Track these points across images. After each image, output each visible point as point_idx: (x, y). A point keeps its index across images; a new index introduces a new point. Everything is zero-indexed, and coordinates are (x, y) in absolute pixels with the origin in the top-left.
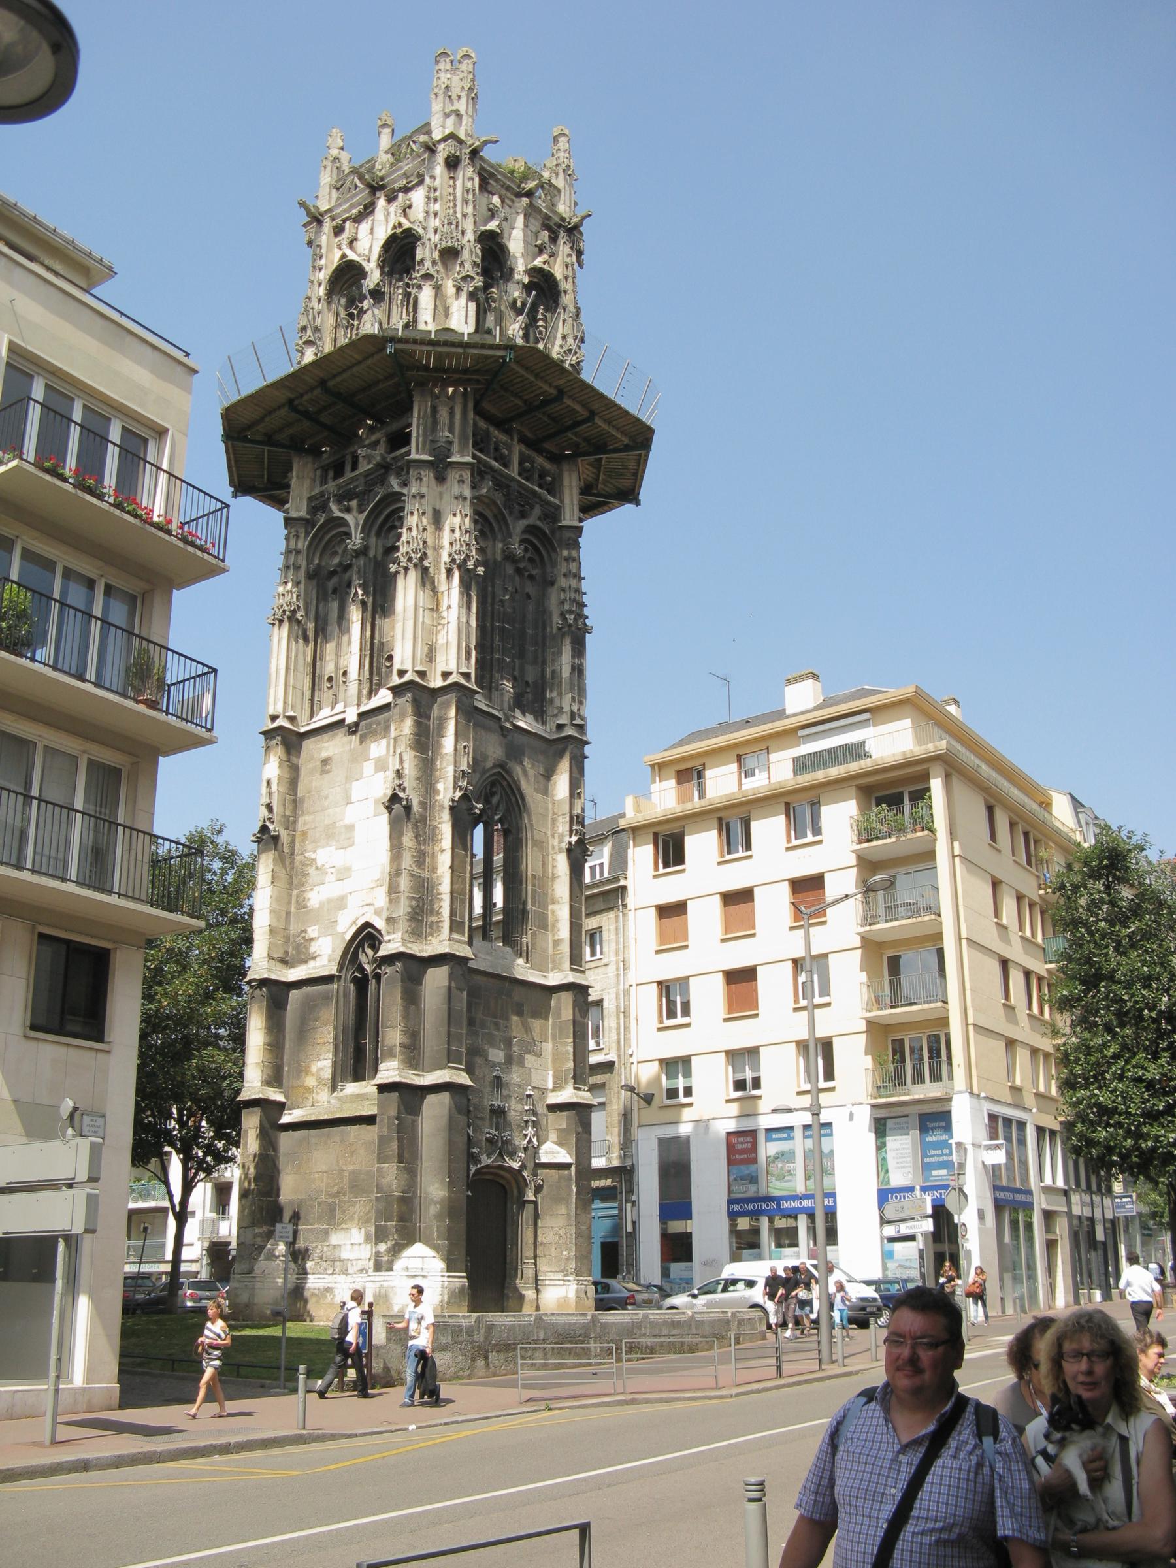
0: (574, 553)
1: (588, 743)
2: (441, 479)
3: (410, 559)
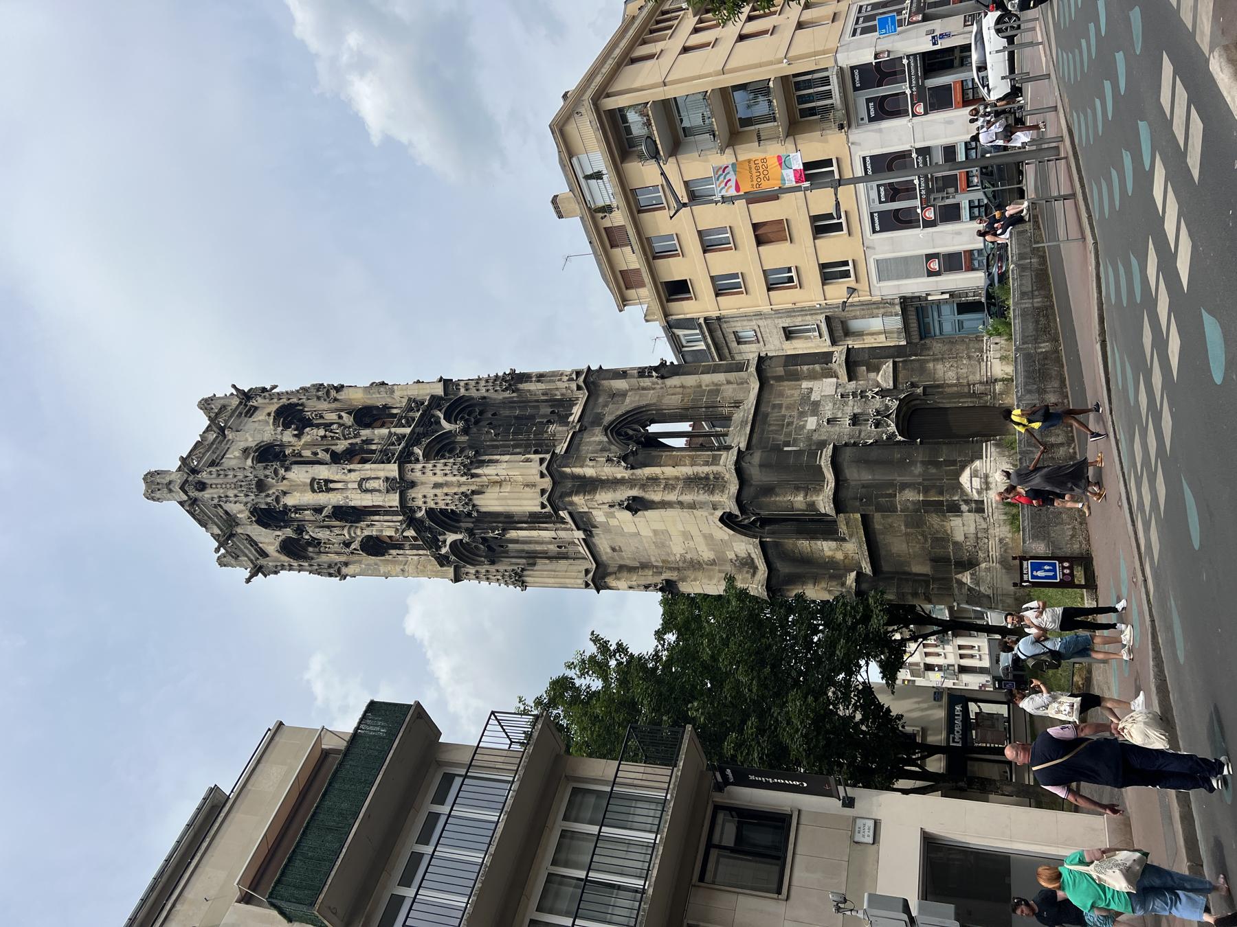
0: (462, 384)
2: (413, 484)
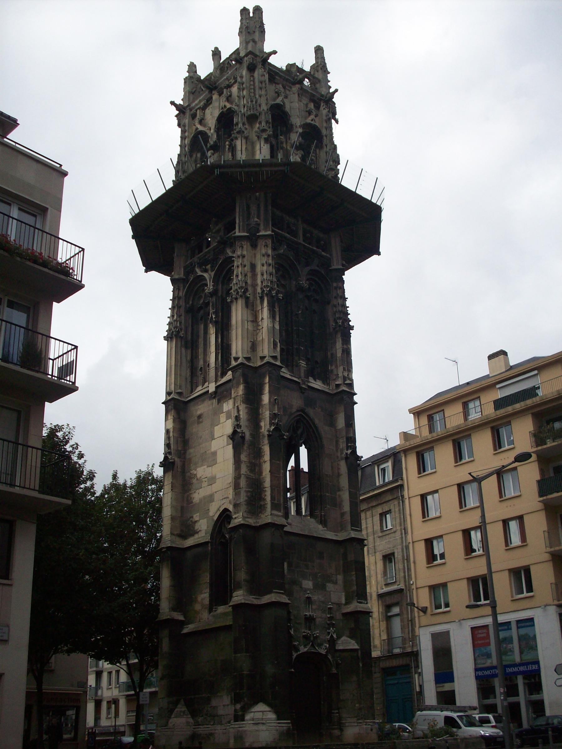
1: (356, 394)
2: (254, 246)
3: (238, 293)
